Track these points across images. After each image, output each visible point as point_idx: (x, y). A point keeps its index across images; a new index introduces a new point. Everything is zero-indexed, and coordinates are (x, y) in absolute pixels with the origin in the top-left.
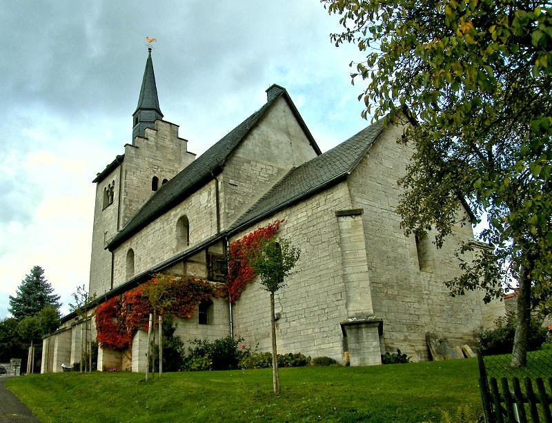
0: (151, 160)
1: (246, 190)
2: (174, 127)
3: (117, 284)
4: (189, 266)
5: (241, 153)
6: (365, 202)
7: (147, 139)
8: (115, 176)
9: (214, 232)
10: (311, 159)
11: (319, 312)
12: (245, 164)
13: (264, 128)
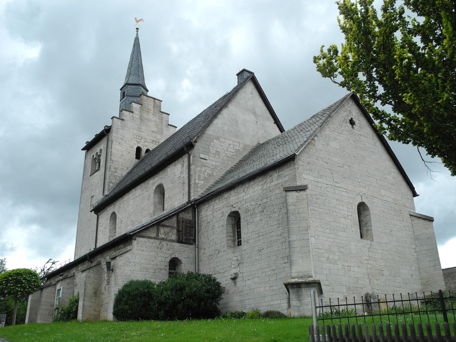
0: (135, 132)
1: (214, 163)
3: (99, 245)
4: (162, 230)
5: (210, 131)
6: (311, 178)
7: (132, 112)
8: (102, 145)
9: (186, 200)
10: (274, 136)
11: (269, 273)
12: (215, 141)
13: (232, 107)
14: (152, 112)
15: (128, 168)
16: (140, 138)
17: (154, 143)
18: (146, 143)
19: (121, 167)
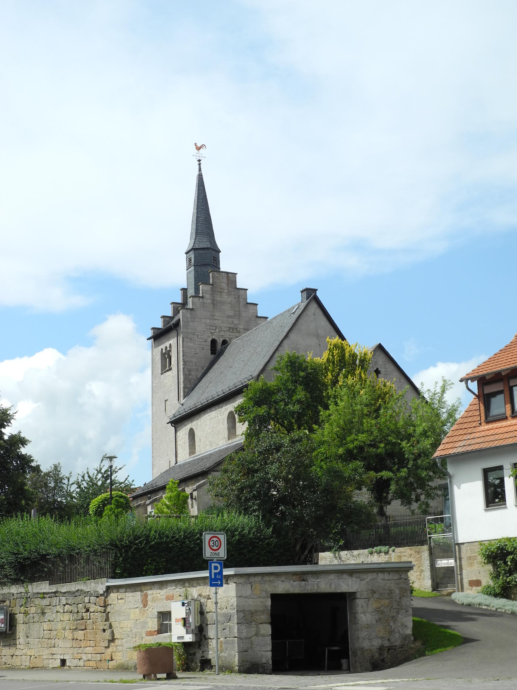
0: (208, 321)
2: (231, 277)
14: (226, 291)
15: (203, 369)
16: (214, 328)
17: (231, 330)
18: (222, 333)
19: (196, 368)
